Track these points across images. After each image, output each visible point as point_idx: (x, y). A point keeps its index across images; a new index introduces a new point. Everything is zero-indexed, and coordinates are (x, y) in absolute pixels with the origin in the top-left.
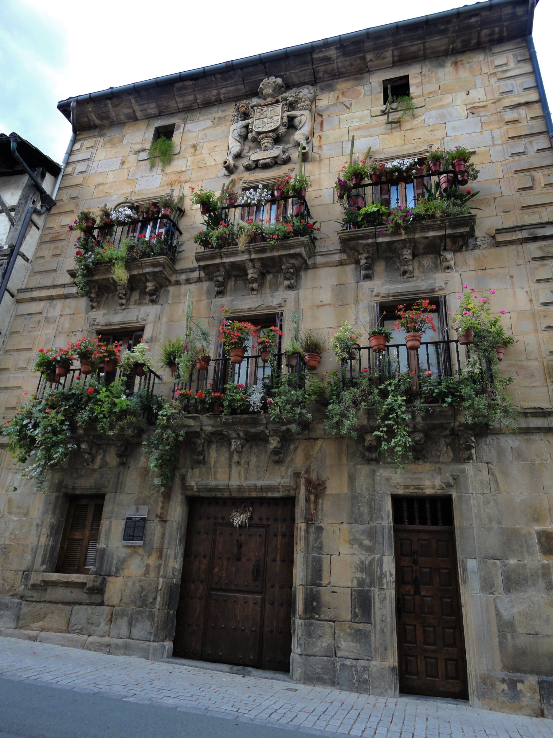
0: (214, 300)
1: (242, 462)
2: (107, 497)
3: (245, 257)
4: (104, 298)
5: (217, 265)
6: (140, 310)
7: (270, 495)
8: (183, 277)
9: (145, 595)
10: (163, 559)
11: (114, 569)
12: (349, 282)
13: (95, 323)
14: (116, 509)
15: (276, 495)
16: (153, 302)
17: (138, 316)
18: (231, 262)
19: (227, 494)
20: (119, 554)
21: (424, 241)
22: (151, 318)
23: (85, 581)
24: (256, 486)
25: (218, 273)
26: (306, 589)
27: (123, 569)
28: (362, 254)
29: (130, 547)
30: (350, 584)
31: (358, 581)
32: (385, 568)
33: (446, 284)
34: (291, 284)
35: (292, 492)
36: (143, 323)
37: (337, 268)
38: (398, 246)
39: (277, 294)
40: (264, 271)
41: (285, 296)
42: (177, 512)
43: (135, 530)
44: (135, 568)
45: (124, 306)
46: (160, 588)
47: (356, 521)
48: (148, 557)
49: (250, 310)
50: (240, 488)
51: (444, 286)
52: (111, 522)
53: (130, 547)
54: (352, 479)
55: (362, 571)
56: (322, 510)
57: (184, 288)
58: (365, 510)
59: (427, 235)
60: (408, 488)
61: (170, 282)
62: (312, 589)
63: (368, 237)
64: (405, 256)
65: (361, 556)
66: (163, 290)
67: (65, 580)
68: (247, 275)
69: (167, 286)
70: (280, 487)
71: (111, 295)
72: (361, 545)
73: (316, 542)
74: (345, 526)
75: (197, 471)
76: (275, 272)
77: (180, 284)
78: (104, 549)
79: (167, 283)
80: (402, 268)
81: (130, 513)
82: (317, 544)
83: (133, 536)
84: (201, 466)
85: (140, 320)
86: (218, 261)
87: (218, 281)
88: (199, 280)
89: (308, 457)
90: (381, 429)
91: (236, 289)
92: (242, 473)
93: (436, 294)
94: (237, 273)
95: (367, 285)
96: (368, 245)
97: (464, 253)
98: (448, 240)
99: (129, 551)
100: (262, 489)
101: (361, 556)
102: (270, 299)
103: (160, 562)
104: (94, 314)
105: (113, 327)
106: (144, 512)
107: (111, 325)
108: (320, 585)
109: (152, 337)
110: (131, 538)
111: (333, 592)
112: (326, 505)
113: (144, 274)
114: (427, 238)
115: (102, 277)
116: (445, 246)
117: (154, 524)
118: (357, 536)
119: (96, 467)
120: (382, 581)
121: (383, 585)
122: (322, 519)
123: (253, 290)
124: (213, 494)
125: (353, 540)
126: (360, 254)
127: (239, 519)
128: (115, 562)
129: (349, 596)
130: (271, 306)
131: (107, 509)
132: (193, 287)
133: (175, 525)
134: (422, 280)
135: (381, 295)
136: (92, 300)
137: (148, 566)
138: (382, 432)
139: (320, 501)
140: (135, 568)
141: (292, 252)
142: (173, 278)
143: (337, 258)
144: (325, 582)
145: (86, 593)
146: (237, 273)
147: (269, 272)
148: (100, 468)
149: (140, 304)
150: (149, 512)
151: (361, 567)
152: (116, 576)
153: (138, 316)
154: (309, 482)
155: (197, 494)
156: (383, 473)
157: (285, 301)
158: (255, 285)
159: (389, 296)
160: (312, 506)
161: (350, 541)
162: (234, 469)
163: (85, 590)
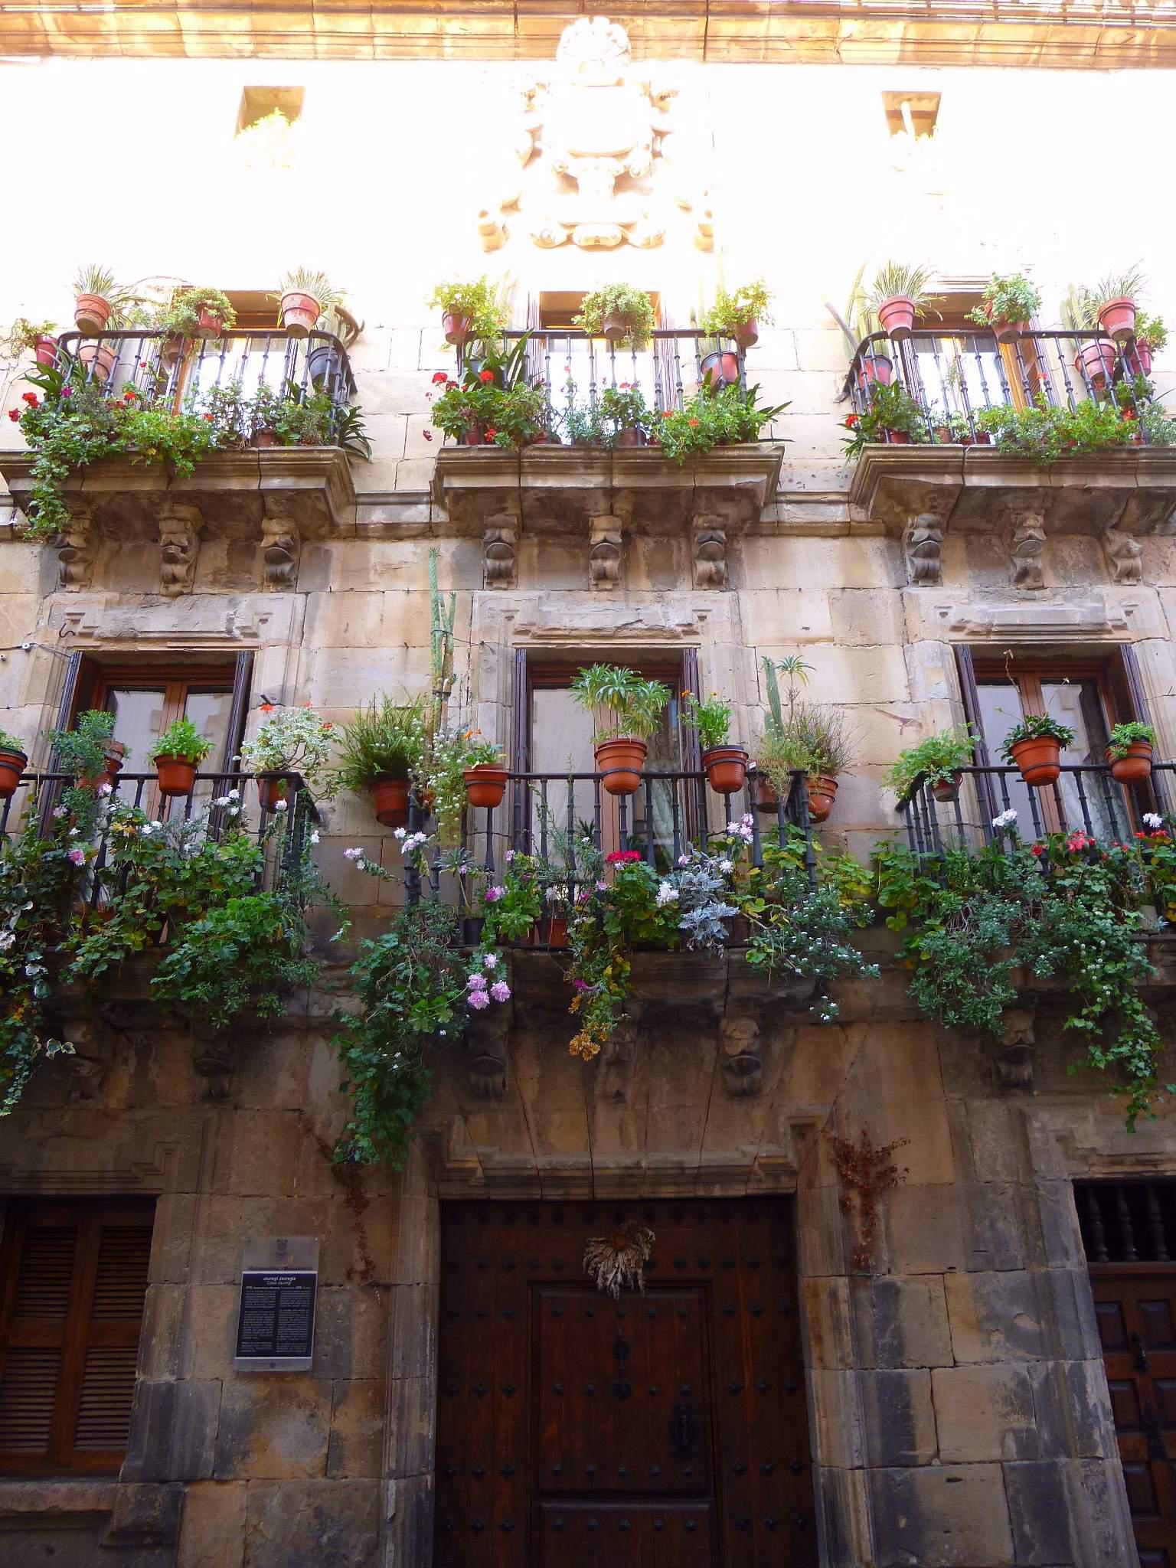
0: (478, 594)
1: (629, 1094)
2: (164, 1210)
3: (594, 481)
4: (104, 555)
5: (501, 494)
6: (233, 603)
7: (717, 1191)
8: (378, 516)
9: (333, 1542)
10: (394, 1413)
11: (210, 1455)
12: (876, 583)
13: (79, 629)
14: (203, 1251)
15: (738, 1191)
16: (281, 582)
17: (230, 620)
18: (549, 490)
19: (581, 1193)
20: (226, 1404)
21: (1079, 499)
22: (276, 630)
23: (103, 1507)
24: (681, 1167)
25: (498, 518)
26: (872, 1479)
27: (245, 1454)
28: (917, 513)
29: (264, 1377)
30: (996, 1453)
31: (1018, 1440)
32: (1092, 1400)
33: (1128, 613)
34: (718, 572)
35: (786, 1184)
36: (247, 642)
37: (838, 542)
38: (1010, 501)
39: (674, 595)
40: (633, 527)
41: (702, 605)
42: (417, 1255)
43: (274, 1320)
44: (290, 1446)
45: (176, 587)
46: (390, 1514)
47: (990, 1263)
48: (334, 1410)
49: (597, 633)
50: (629, 1176)
51: (1125, 619)
52: (187, 1294)
53: (264, 1377)
54: (962, 1141)
55: (1026, 1409)
56: (888, 1235)
57: (378, 551)
58: (1009, 1229)
59: (1091, 484)
60: (1120, 1163)
61: (333, 525)
62: (888, 1478)
63: (940, 468)
64: (1031, 532)
65: (1016, 1365)
66: (307, 548)
67: (23, 1508)
68: (586, 531)
69: (322, 538)
70: (756, 1167)
71: (128, 546)
72: (1013, 1334)
73: (883, 1331)
74: (961, 1279)
75: (480, 1121)
76: (662, 535)
77: (366, 538)
78: (171, 1388)
79: (324, 530)
80: (1019, 562)
81: (257, 1261)
82: (887, 1339)
83: (273, 1339)
84: (494, 1105)
85: (237, 633)
86: (507, 482)
87: (499, 539)
88: (428, 531)
89: (827, 1078)
90: (1085, 1011)
91: (544, 569)
92: (631, 1128)
93: (1108, 638)
94: (551, 523)
95: (926, 596)
96: (941, 490)
97: (1158, 540)
98: (1133, 505)
99: (258, 1390)
100: (700, 1176)
101: (1016, 1365)
102: (657, 608)
103: (379, 1424)
104: (70, 599)
105: (141, 647)
106: (305, 1257)
107: (135, 639)
108: (910, 1463)
109: (283, 690)
110: (268, 1345)
111: (949, 1480)
112: (898, 1215)
113: (261, 494)
114: (1089, 490)
115: (118, 487)
116: (1121, 517)
117: (345, 1298)
118: (999, 1305)
119: (113, 1104)
120: (1090, 1436)
121: (1095, 1448)
122: (892, 1261)
123: (603, 576)
124: (536, 1193)
125: (987, 1318)
126: (908, 510)
127: (613, 1268)
128: (210, 1431)
129: (999, 1487)
130: (662, 629)
131: (167, 1248)
132: (405, 551)
133: (417, 1295)
134: (1066, 599)
135: (969, 626)
136: (67, 557)
137: (334, 1441)
138: (1087, 1018)
139: (880, 1208)
140: (290, 1446)
141: (733, 481)
142: (345, 518)
143: (838, 514)
144: (924, 1451)
145: (105, 1548)
146: (551, 523)
147: (643, 532)
148: (130, 1108)
149: (232, 584)
150: (322, 1255)
151: (1022, 1398)
152: (221, 1482)
153: (230, 620)
154: (844, 1155)
155: (480, 1194)
156: (1048, 1121)
157: (702, 618)
158: (610, 565)
159: (989, 633)
160: (857, 1222)
161: (979, 1322)
162: (604, 1117)
163: (104, 1538)
